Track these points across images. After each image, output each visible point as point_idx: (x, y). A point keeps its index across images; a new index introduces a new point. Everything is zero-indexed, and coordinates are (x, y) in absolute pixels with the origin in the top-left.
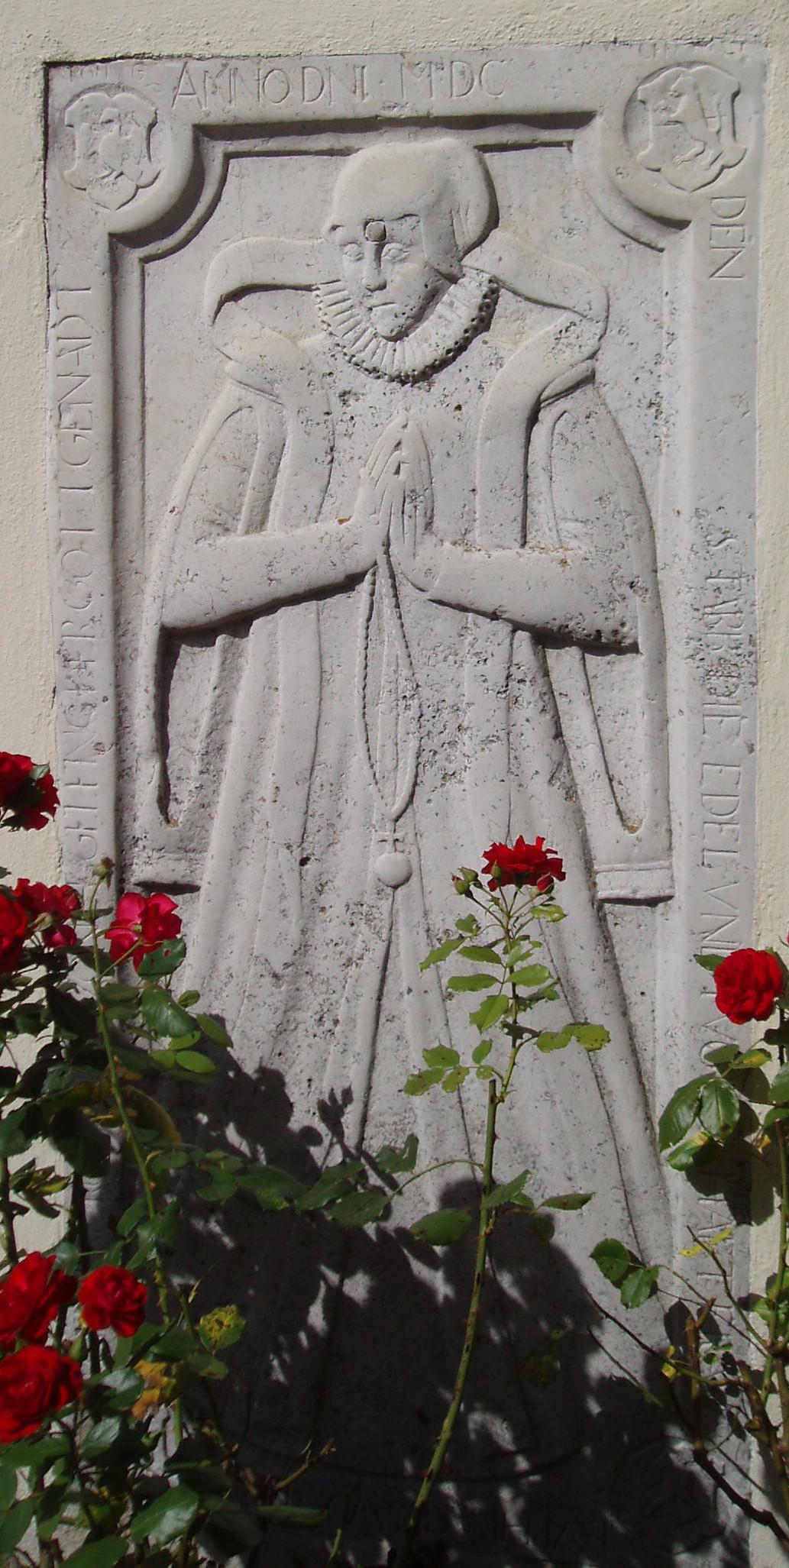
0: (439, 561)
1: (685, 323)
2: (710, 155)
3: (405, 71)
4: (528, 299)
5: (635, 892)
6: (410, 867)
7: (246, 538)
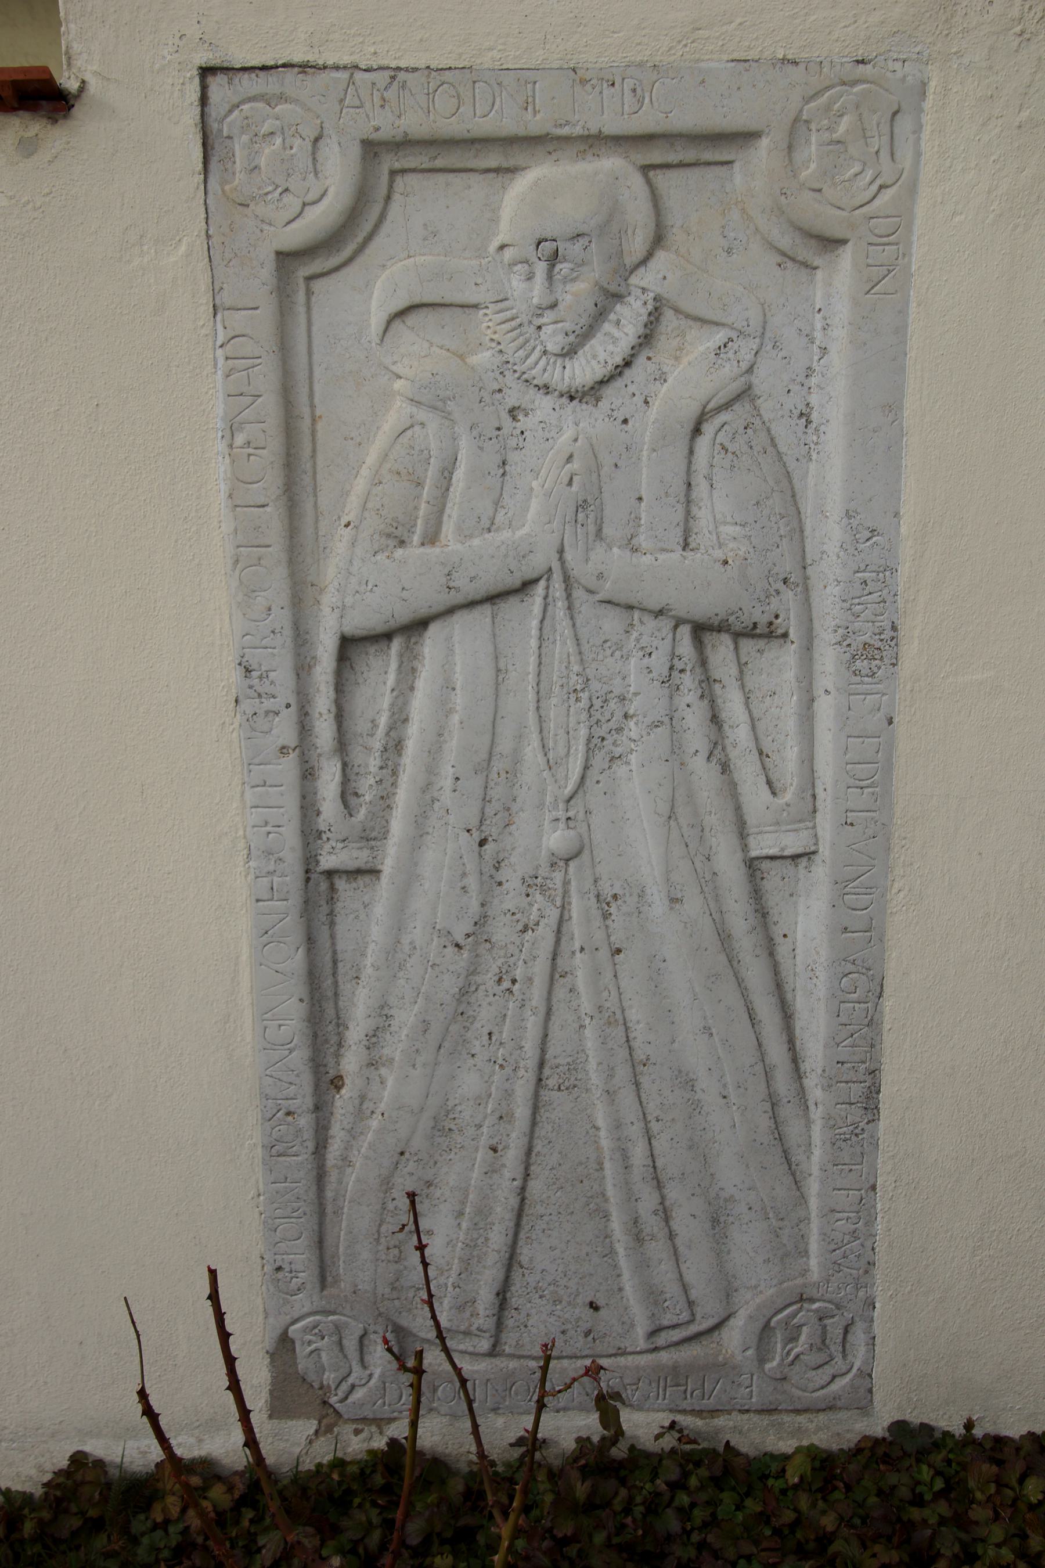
0: (611, 565)
1: (839, 337)
2: (869, 175)
3: (578, 88)
4: (688, 316)
5: (783, 849)
6: (582, 841)
7: (422, 549)
